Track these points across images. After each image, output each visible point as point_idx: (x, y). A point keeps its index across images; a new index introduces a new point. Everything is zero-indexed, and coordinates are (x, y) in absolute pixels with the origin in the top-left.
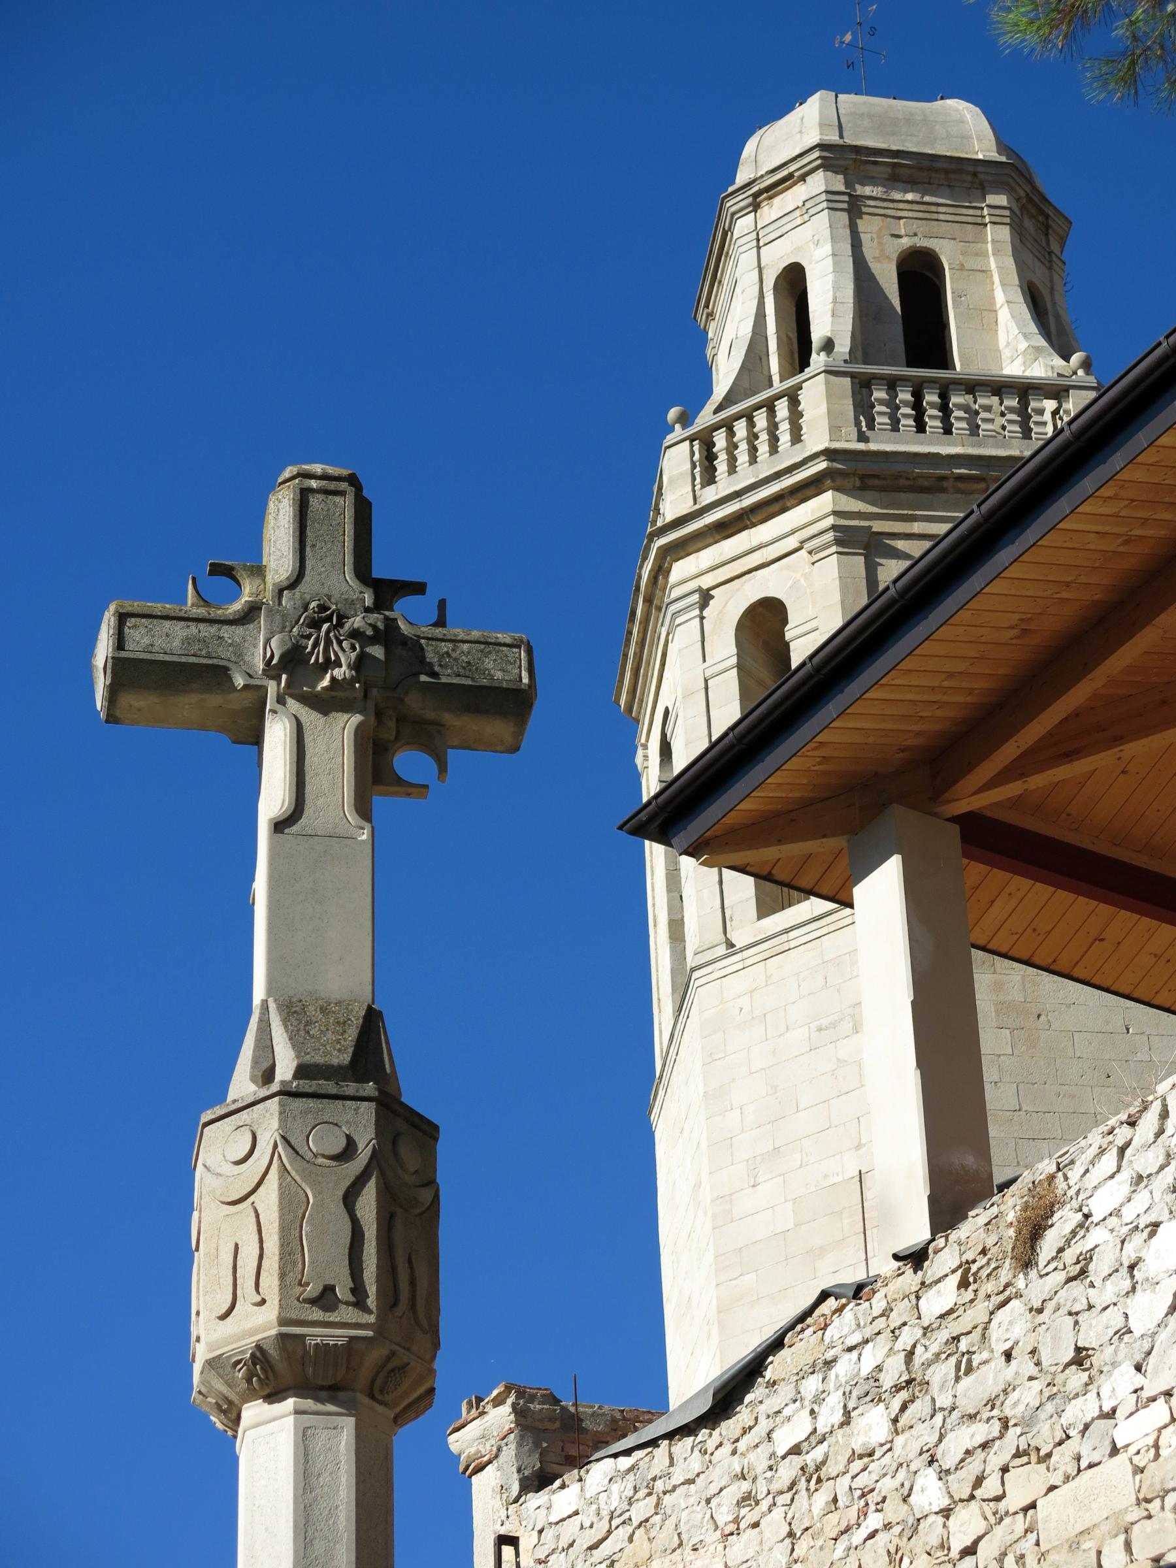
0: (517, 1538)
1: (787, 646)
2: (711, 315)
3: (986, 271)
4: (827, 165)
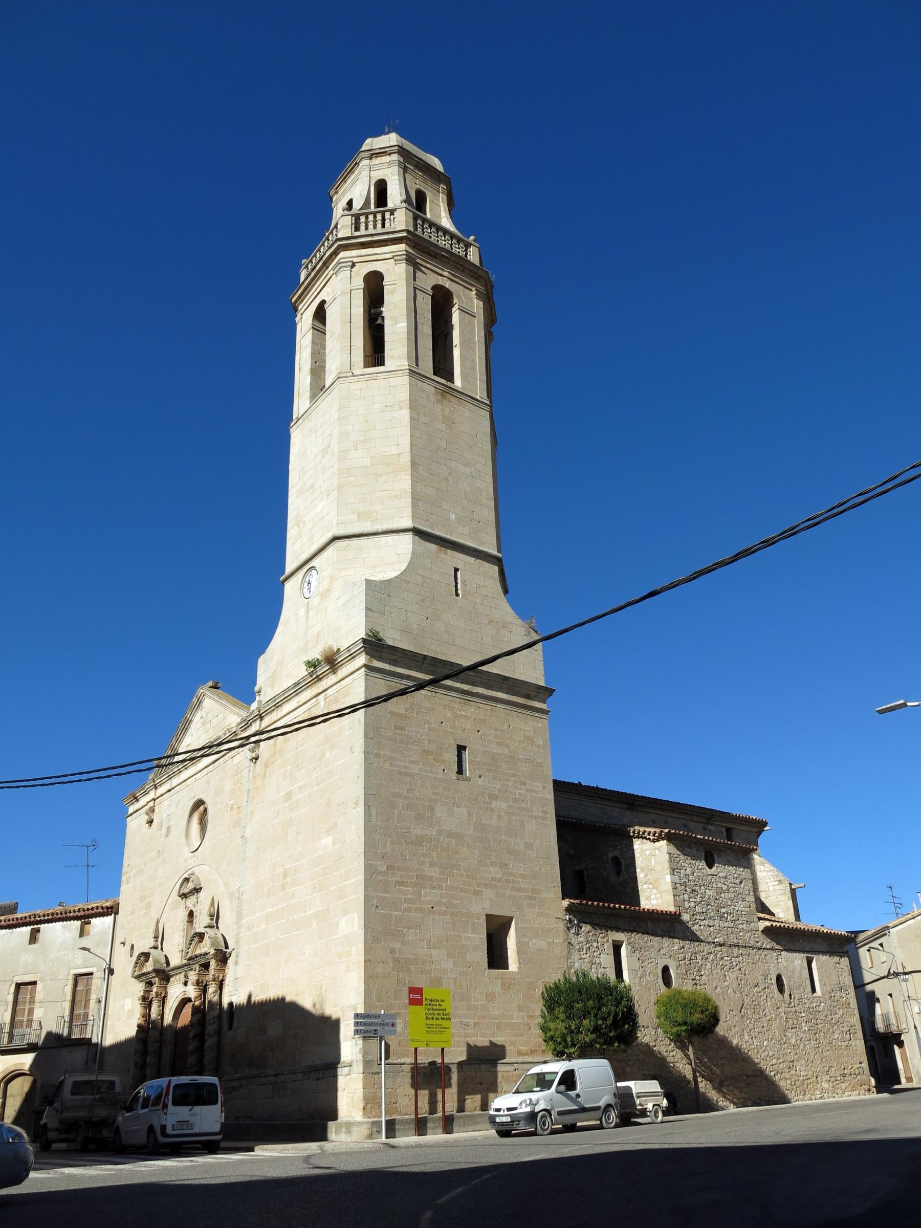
0: (422, 989)
1: (383, 287)
2: (336, 192)
3: (439, 205)
4: (399, 153)
